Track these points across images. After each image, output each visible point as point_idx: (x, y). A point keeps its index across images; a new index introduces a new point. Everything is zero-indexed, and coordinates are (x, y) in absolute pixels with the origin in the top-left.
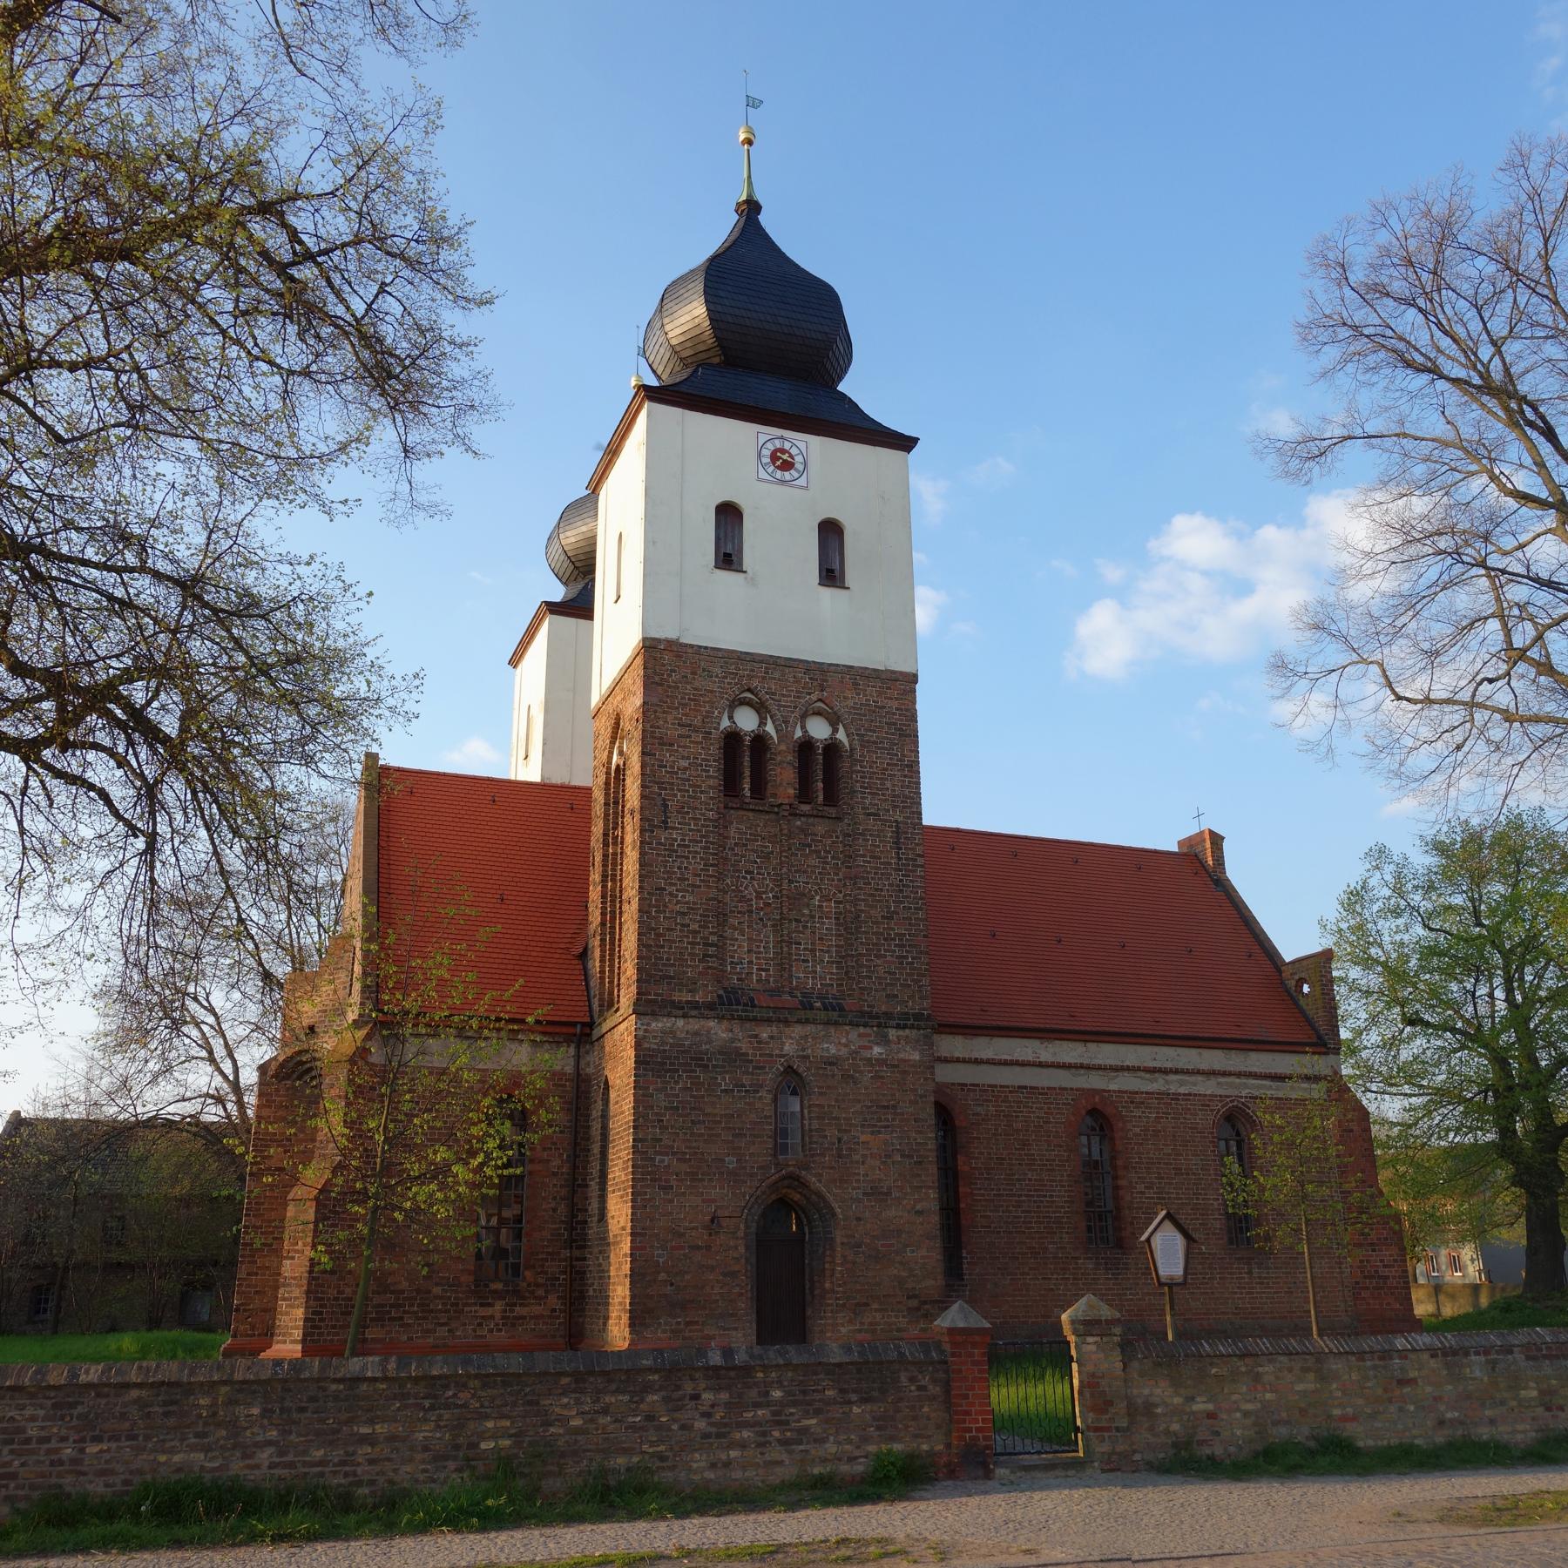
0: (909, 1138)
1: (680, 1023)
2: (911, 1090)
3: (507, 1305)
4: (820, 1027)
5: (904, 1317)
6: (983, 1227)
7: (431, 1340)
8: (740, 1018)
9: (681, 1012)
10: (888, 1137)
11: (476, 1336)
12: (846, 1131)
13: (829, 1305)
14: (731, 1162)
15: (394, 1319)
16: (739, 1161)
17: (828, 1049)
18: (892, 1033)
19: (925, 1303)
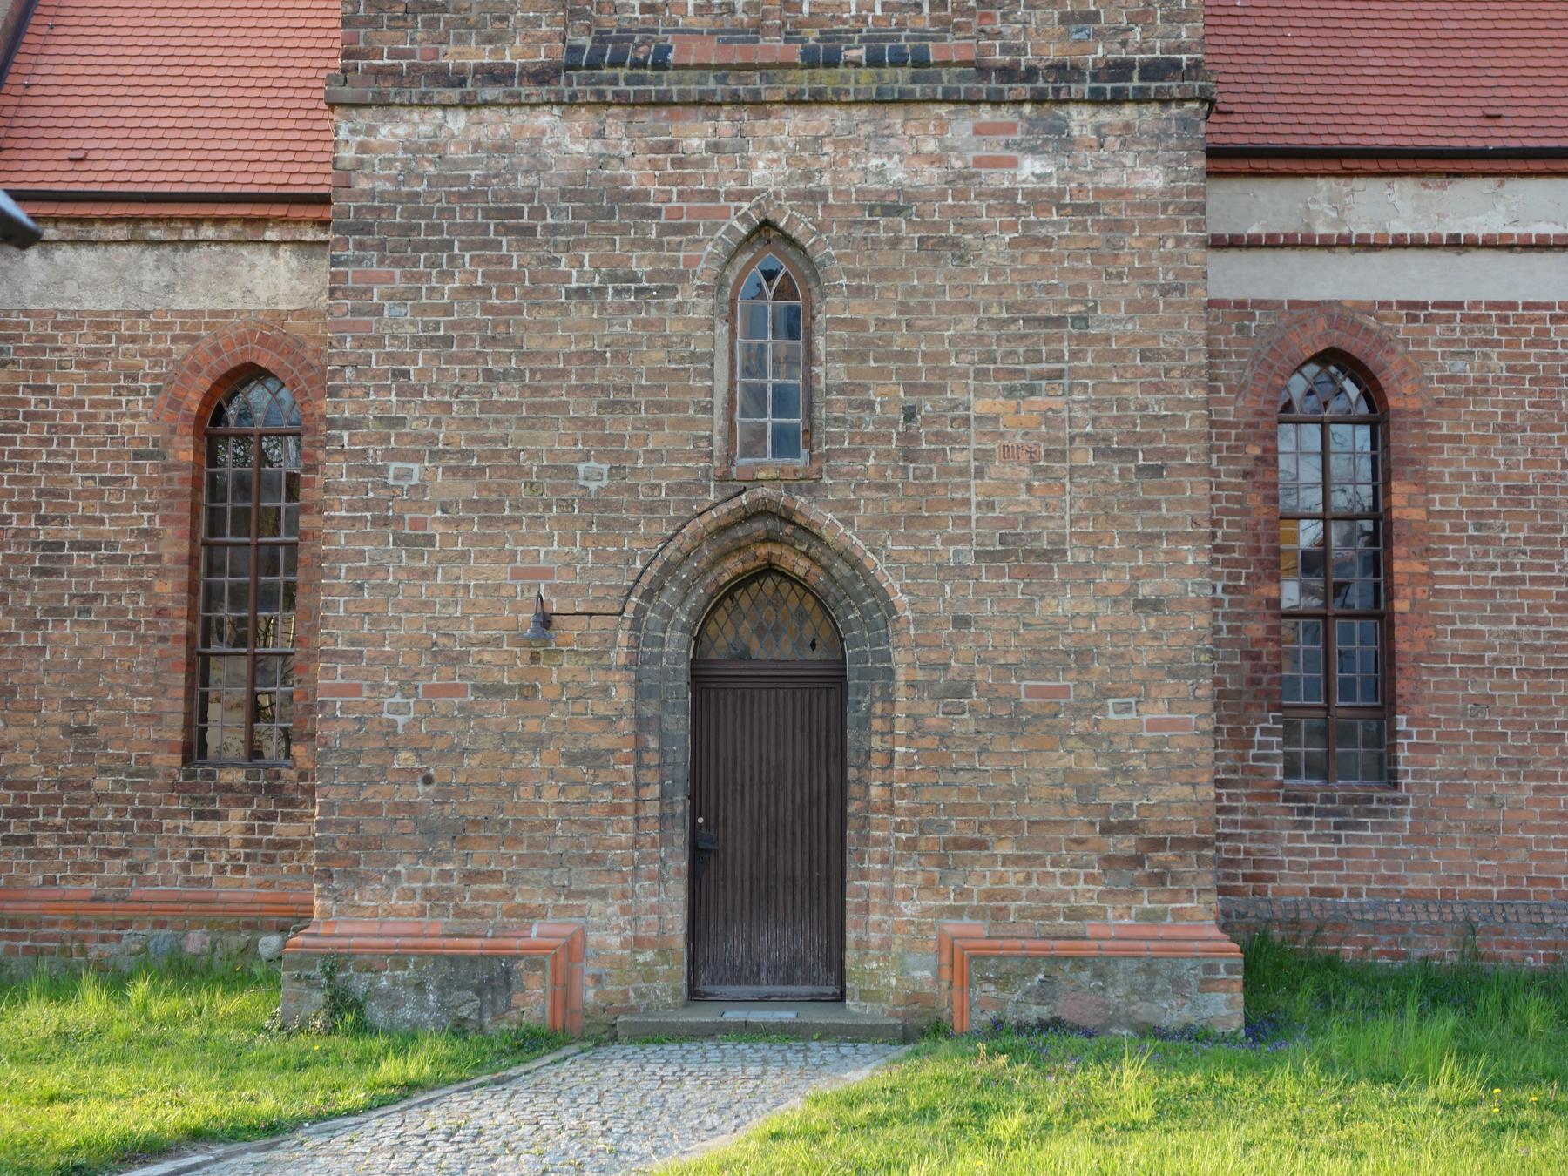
0: (1122, 405)
1: (457, 122)
2: (1134, 273)
3: (254, 816)
4: (860, 113)
5: (1090, 879)
6: (1456, 658)
7: (92, 886)
8: (621, 101)
9: (455, 95)
10: (1057, 403)
11: (188, 881)
12: (929, 389)
13: (877, 842)
14: (594, 475)
15: (16, 840)
16: (615, 471)
17: (881, 173)
18: (1081, 120)
19: (1158, 844)
